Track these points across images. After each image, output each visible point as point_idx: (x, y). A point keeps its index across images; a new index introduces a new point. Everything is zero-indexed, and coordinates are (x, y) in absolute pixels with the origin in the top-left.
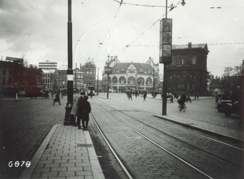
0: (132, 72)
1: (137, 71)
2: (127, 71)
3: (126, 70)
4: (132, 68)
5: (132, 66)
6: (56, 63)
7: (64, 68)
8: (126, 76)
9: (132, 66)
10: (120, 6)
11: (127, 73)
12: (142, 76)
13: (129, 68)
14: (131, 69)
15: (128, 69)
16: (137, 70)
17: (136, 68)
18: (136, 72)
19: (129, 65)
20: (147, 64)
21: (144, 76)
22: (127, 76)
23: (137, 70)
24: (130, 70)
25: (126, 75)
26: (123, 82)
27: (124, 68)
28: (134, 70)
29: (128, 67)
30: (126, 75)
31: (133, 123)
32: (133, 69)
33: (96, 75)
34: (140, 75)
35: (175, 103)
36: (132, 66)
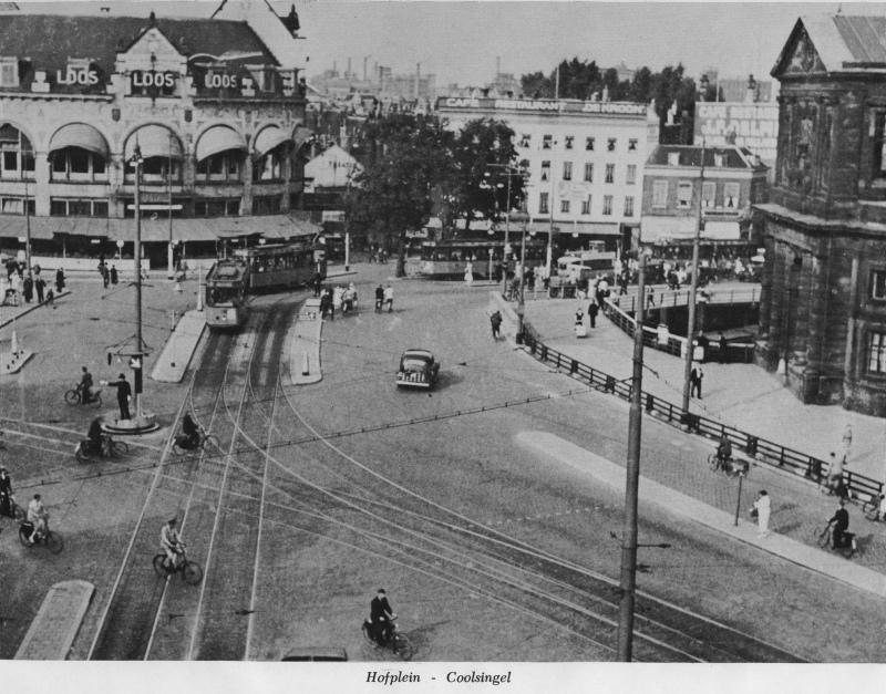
0: (154, 92)
2: (119, 85)
3: (104, 72)
5: (155, 41)
6: (566, 164)
7: (313, 477)
9: (153, 46)
10: (293, 7)
14: (146, 66)
15: (120, 68)
18: (186, 87)
20: (220, 22)
21: (242, 113)
22: (116, 116)
24: (140, 73)
27: (85, 63)
28: (176, 75)
29: (124, 52)
30: (107, 109)
31: (401, 560)
32: (160, 67)
33: (520, 230)
34: (216, 114)
35: (569, 255)
36: (155, 41)
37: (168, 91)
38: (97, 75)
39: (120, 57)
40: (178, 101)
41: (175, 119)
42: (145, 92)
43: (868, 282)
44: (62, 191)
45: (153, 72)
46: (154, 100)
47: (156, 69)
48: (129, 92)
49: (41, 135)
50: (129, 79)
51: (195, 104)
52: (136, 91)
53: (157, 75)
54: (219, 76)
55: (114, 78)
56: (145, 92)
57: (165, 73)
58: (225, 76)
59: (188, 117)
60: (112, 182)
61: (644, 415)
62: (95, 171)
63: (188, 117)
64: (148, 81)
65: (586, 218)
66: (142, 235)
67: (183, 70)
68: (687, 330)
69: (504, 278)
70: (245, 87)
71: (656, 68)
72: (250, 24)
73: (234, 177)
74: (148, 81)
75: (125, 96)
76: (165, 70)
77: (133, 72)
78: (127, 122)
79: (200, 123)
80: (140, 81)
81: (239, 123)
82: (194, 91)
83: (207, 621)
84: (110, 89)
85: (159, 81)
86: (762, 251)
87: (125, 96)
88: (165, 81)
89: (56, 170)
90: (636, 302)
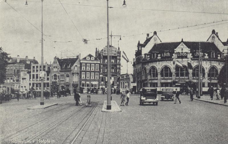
2: (174, 56)
4: (182, 49)
9: (182, 47)
12: (154, 64)
13: (178, 50)
14: (180, 51)
15: (175, 52)
16: (190, 53)
17: (190, 49)
18: (190, 56)
19: (176, 45)
20: (209, 43)
22: (174, 63)
23: (190, 53)
24: (179, 53)
25: (172, 62)
28: (187, 53)
29: (176, 48)
30: (172, 62)
32: (184, 51)
37: (186, 57)
38: (170, 54)
39: (175, 49)
40: (188, 59)
44: (163, 81)
45: (182, 53)
46: (127, 73)
47: (183, 52)
48: (177, 57)
49: (159, 68)
52: (178, 57)
54: (198, 53)
55: (174, 54)
57: (185, 53)
61: (200, 99)
64: (181, 54)
65: (131, 83)
67: (189, 52)
68: (155, 89)
69: (46, 86)
73: (156, 78)
74: (181, 54)
75: (176, 59)
76: (185, 52)
77: (178, 53)
79: (161, 65)
80: (179, 54)
81: (157, 65)
82: (192, 57)
83: (15, 62)
84: (173, 57)
85: (167, 55)
89: (162, 77)
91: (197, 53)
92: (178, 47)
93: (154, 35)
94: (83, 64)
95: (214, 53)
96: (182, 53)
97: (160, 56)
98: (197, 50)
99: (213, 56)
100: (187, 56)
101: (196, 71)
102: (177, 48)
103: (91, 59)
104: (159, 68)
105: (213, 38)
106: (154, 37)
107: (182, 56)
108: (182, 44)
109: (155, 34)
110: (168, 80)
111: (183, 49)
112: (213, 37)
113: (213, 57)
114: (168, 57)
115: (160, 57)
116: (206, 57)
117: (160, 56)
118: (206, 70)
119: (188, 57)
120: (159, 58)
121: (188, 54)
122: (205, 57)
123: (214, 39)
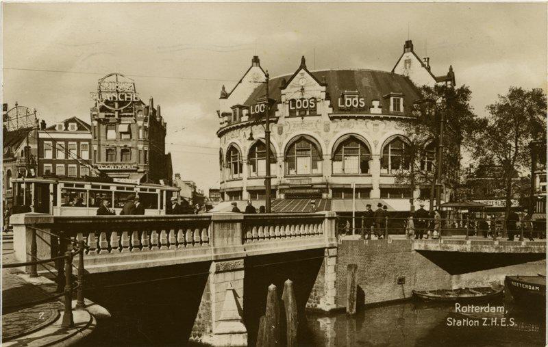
1: (328, 102)
2: (282, 110)
4: (303, 90)
8: (323, 133)
9: (302, 83)
10: (451, 69)
11: (281, 121)
13: (290, 93)
14: (297, 96)
15: (283, 100)
17: (324, 88)
18: (324, 108)
24: (293, 101)
26: (353, 163)
29: (284, 88)
32: (307, 96)
34: (348, 126)
36: (304, 79)
37: (313, 112)
41: (316, 130)
42: (297, 113)
43: (27, 331)
46: (303, 118)
47: (304, 97)
48: (288, 114)
50: (288, 105)
51: (332, 119)
52: (292, 114)
53: (304, 101)
55: (279, 106)
56: (297, 113)
58: (356, 106)
59: (327, 130)
60: (278, 176)
62: (403, 168)
63: (327, 130)
66: (20, 223)
67: (323, 96)
70: (373, 107)
71: (528, 89)
72: (411, 79)
75: (286, 117)
78: (287, 135)
79: (335, 132)
82: (330, 110)
84: (277, 114)
86: (377, 238)
87: (286, 117)
88: (310, 104)
90: (73, 339)
91: (347, 99)
92: (291, 83)
93: (404, 52)
94: (45, 142)
95: (402, 99)
96: (302, 99)
97: (247, 115)
98: (346, 91)
99: (397, 106)
100: (315, 108)
101: (232, 159)
102: (288, 87)
103: (69, 128)
104: (327, 141)
105: (408, 65)
106: (404, 58)
107: (303, 110)
108: (302, 74)
109: (255, 64)
110: (313, 178)
111: (306, 89)
112: (408, 62)
113: (399, 109)
114: (360, 109)
115: (380, 109)
116: (376, 110)
117: (247, 115)
118: (327, 148)
119: (318, 113)
120: (245, 119)
121: (318, 103)
122: (372, 111)
123: (409, 67)
